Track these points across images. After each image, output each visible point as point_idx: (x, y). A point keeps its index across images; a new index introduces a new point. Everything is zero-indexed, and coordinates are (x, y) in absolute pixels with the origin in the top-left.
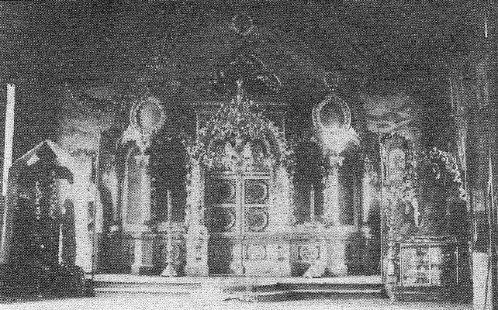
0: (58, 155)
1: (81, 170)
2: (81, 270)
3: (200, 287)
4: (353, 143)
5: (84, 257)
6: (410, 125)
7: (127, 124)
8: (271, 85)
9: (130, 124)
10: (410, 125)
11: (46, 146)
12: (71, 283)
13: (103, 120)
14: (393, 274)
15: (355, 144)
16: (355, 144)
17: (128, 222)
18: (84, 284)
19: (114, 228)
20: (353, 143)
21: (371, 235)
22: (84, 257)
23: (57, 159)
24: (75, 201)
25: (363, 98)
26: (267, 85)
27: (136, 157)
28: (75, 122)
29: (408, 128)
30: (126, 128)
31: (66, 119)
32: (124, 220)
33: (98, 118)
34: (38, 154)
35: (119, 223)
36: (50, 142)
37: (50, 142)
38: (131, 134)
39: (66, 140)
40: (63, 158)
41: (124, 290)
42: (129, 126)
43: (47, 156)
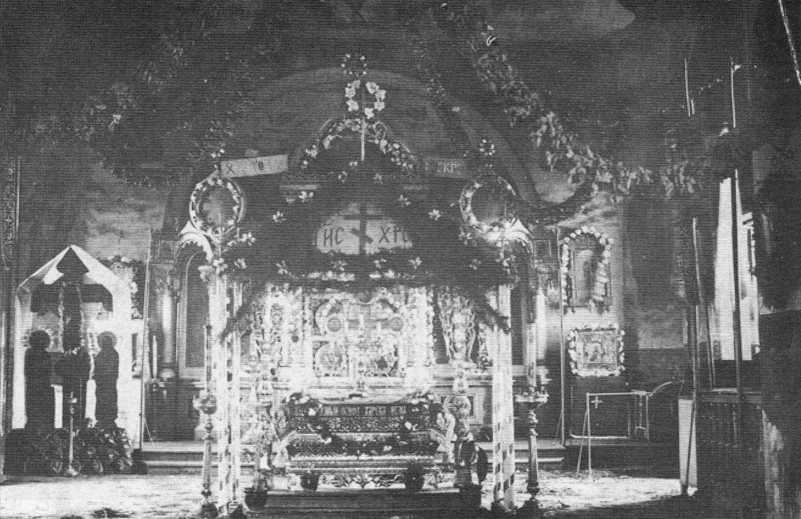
0: (90, 269)
1: (120, 285)
2: (123, 435)
3: (439, 361)
4: (521, 244)
5: (130, 418)
6: (607, 215)
7: (185, 219)
8: (398, 160)
9: (189, 218)
10: (607, 215)
11: (71, 255)
12: (102, 454)
13: (148, 212)
14: (527, 442)
15: (524, 245)
16: (524, 245)
17: (189, 364)
18: (129, 456)
19: (167, 374)
20: (521, 244)
21: (549, 380)
22: (130, 418)
23: (87, 274)
24: (119, 341)
25: (534, 176)
26: (393, 160)
27: (201, 268)
28: (109, 217)
29: (602, 219)
30: (183, 226)
31: (94, 212)
32: (182, 360)
33: (141, 210)
34: (60, 267)
35: (174, 367)
36: (74, 247)
37: (74, 247)
38: (193, 233)
39: (96, 242)
40: (97, 274)
41: (157, 463)
42: (189, 222)
43: (73, 268)
